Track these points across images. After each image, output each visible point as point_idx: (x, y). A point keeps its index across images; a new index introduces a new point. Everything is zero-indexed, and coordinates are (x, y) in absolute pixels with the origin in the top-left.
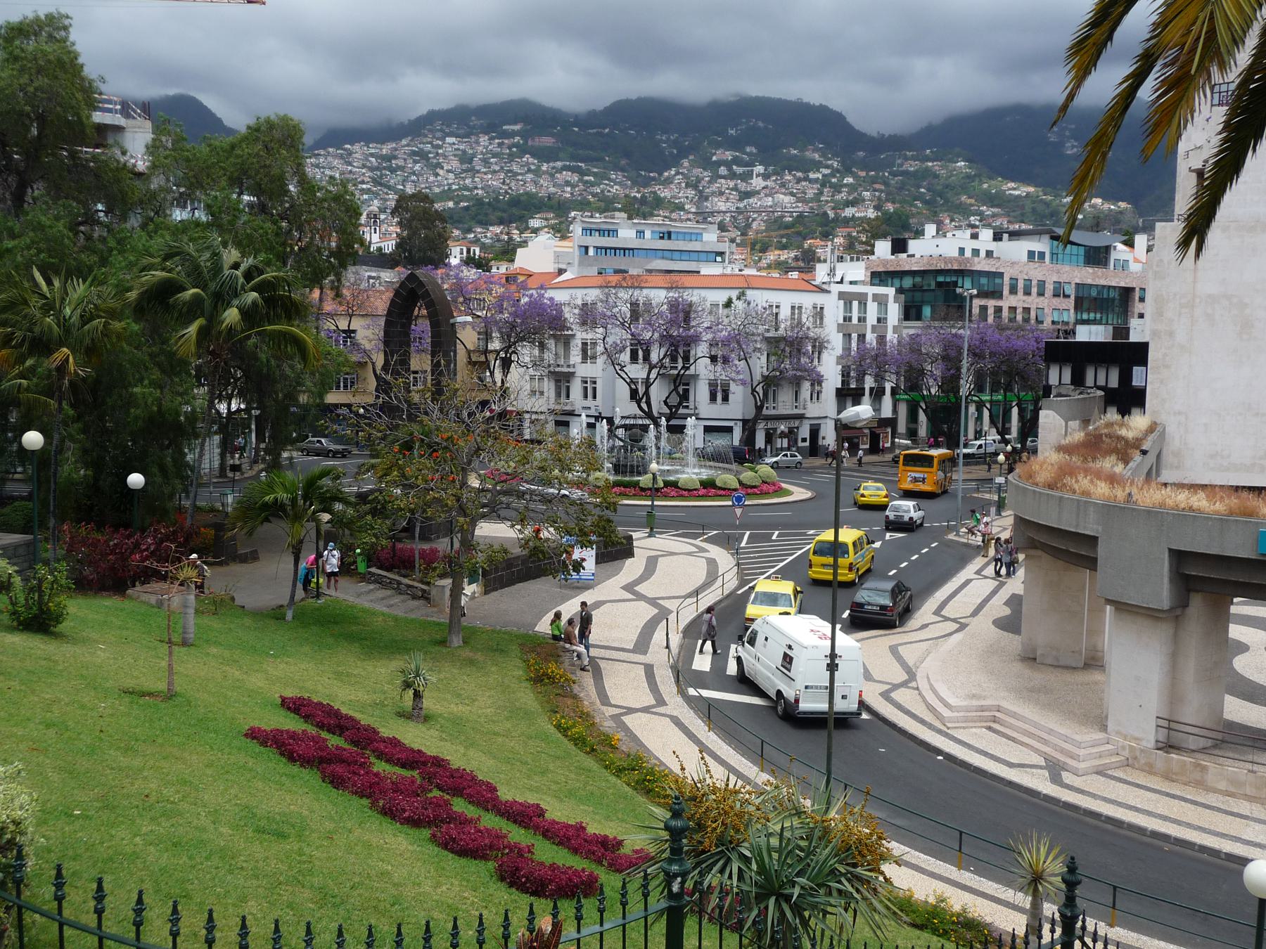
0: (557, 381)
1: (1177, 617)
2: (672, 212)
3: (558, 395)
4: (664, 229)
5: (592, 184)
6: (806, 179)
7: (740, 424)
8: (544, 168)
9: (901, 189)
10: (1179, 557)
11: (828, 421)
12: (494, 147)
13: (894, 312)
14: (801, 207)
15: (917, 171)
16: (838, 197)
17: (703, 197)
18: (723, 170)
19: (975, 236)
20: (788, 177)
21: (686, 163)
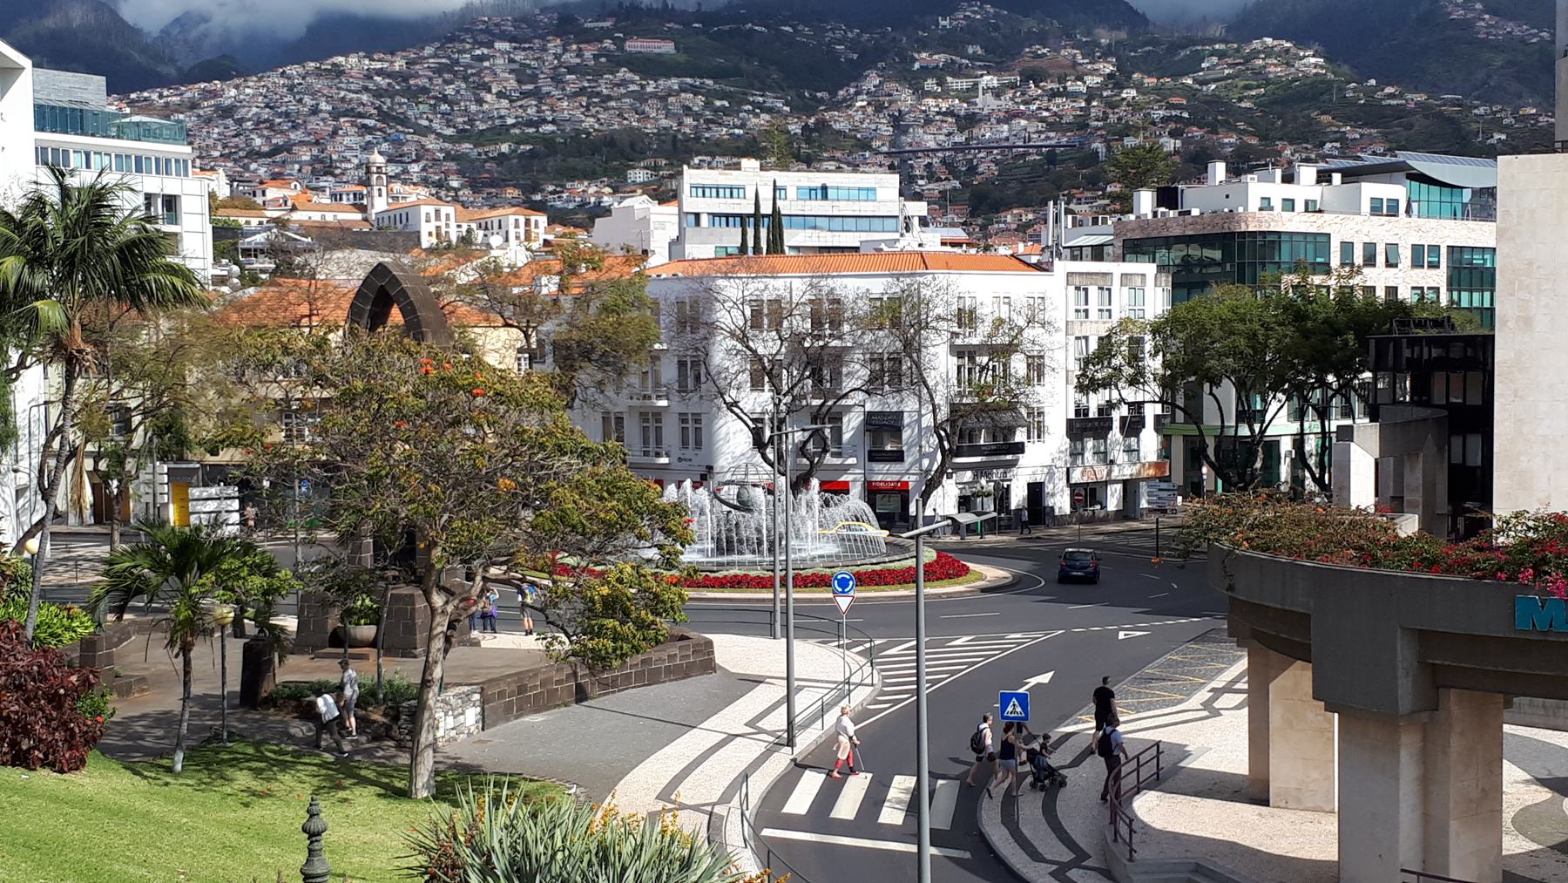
6: (1065, 93)
8: (649, 89)
12: (570, 58)
14: (1054, 138)
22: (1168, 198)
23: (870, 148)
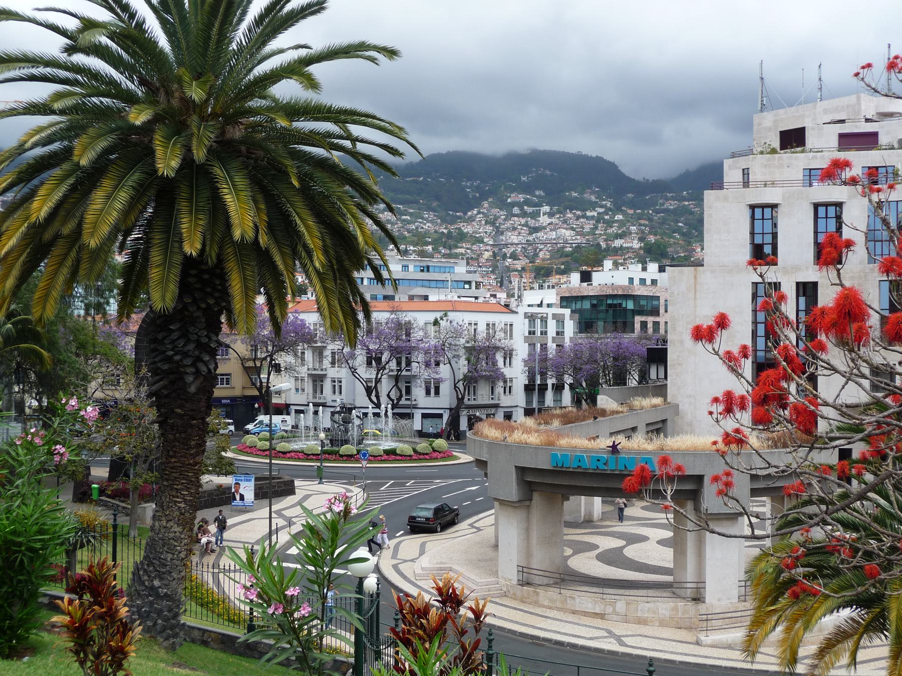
0: (314, 381)
1: (528, 506)
2: (473, 244)
3: (315, 391)
4: (425, 264)
5: (409, 222)
6: (584, 216)
7: (448, 411)
9: (663, 223)
10: (522, 471)
11: (518, 409)
13: (570, 328)
14: (579, 239)
15: (675, 209)
16: (610, 231)
17: (499, 232)
18: (516, 210)
19: (644, 269)
20: (569, 215)
21: (486, 204)
22: (586, 277)
23: (482, 242)
